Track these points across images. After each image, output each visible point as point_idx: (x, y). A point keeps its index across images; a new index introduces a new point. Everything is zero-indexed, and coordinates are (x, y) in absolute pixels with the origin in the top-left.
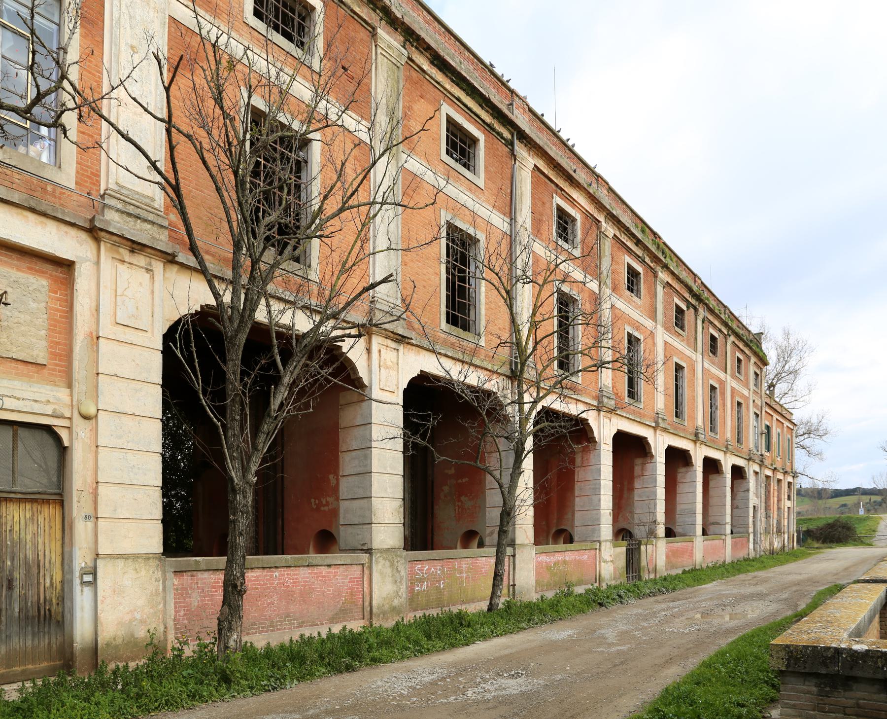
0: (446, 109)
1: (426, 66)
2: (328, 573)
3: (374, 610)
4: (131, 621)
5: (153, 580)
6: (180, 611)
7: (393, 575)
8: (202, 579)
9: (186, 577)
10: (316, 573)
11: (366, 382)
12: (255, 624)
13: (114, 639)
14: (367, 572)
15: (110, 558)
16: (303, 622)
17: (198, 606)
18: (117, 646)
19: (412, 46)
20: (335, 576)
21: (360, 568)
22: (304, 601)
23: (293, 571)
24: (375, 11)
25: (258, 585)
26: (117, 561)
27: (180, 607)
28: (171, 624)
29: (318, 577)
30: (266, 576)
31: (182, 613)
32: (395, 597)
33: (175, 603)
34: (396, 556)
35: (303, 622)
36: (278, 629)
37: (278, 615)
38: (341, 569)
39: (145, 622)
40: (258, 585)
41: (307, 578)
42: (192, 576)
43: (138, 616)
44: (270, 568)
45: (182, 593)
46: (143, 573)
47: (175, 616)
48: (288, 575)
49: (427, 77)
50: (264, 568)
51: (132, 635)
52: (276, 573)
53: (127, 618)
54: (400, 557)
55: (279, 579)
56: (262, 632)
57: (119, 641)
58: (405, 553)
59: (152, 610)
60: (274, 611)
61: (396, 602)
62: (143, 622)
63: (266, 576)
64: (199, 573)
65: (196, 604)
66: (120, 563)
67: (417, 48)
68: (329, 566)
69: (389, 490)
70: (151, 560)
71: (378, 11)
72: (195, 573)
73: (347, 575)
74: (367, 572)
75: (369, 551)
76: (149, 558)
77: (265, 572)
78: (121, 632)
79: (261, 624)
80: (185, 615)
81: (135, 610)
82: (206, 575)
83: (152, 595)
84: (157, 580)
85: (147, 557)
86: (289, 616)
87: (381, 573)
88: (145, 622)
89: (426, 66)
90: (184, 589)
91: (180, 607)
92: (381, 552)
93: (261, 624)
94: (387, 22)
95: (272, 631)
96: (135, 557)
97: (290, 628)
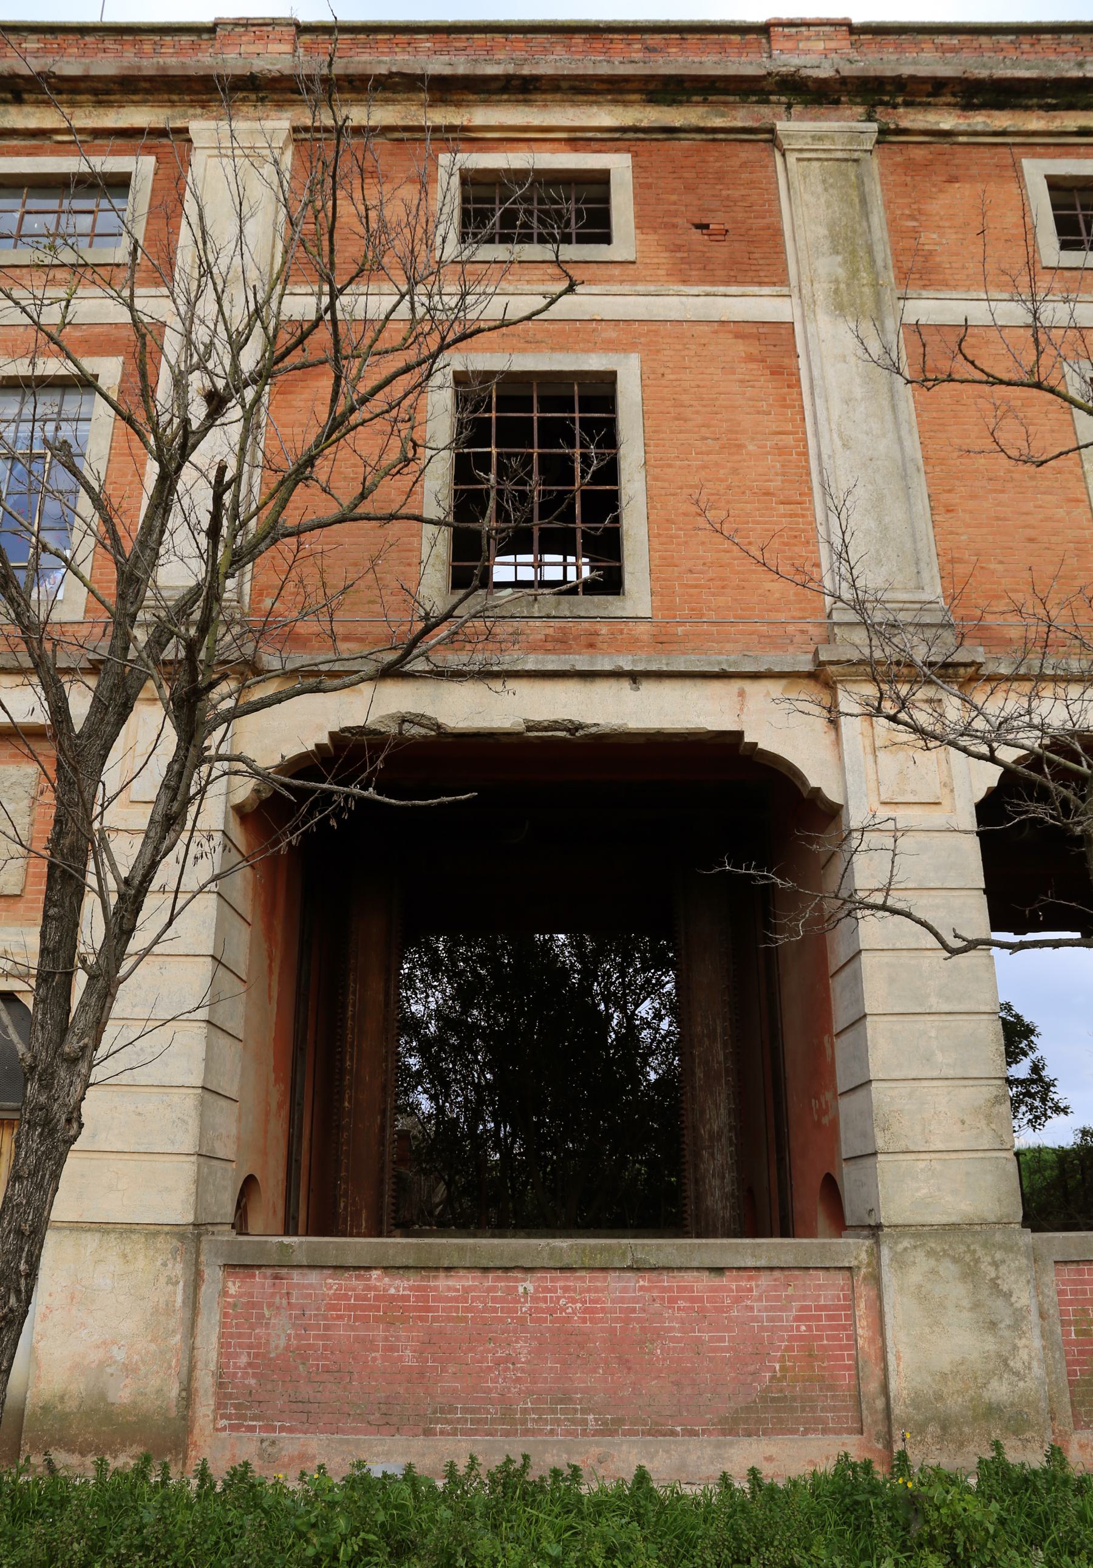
0: (1036, 171)
1: (948, 121)
2: (713, 1289)
3: (898, 1410)
4: (101, 1365)
5: (163, 1280)
6: (237, 1355)
7: (976, 1306)
8: (304, 1286)
9: (260, 1280)
10: (664, 1289)
11: (833, 794)
12: (453, 1410)
13: (62, 1398)
14: (864, 1292)
15: (71, 1230)
16: (619, 1421)
17: (287, 1348)
18: (64, 1416)
19: (895, 106)
20: (738, 1300)
21: (840, 1279)
22: (623, 1362)
23: (583, 1281)
24: (767, 102)
25: (467, 1310)
26: (84, 1235)
27: (240, 1345)
28: (205, 1381)
29: (673, 1300)
30: (493, 1289)
31: (243, 1360)
32: (990, 1374)
33: (222, 1335)
34: (985, 1245)
35: (619, 1421)
36: (526, 1432)
37: (530, 1392)
38: (765, 1280)
39: (136, 1370)
40: (467, 1310)
41: (635, 1300)
42: (276, 1277)
43: (120, 1355)
44: (506, 1269)
45: (241, 1321)
46: (141, 1263)
47: (220, 1366)
48: (566, 1289)
49: (961, 139)
50: (486, 1269)
51: (103, 1396)
52: (527, 1285)
53: (95, 1356)
54: (1009, 1248)
55: (535, 1299)
56: (474, 1432)
57: (71, 1405)
58: (1028, 1237)
59: (153, 1347)
60: (518, 1380)
61: (999, 1390)
62: (129, 1369)
63: (493, 1289)
64: (296, 1275)
65: (282, 1343)
66: (91, 1241)
67: (907, 104)
68: (719, 1270)
69: (939, 1057)
70: (161, 1238)
71: (773, 98)
72: (284, 1271)
73: (790, 1298)
74: (864, 1292)
75: (875, 1230)
76: (156, 1234)
77: (490, 1280)
78: (79, 1386)
79: (472, 1411)
80: (250, 1365)
81: (114, 1343)
82: (313, 1278)
83: (156, 1311)
84: (172, 1282)
85: (152, 1231)
86: (566, 1399)
87: (922, 1297)
88: (136, 1370)
89: (948, 121)
90: (252, 1305)
91: (240, 1345)
92: (915, 1236)
93: (472, 1411)
94: (806, 103)
95: (507, 1434)
96: (126, 1230)
97: (568, 1433)
